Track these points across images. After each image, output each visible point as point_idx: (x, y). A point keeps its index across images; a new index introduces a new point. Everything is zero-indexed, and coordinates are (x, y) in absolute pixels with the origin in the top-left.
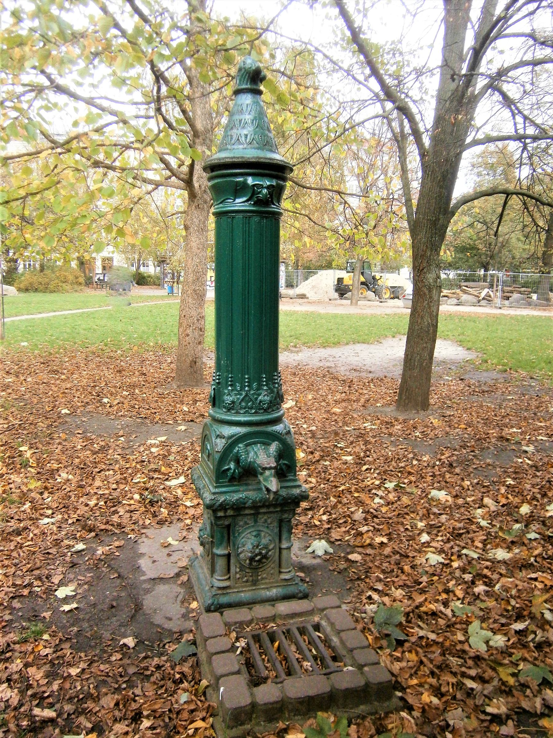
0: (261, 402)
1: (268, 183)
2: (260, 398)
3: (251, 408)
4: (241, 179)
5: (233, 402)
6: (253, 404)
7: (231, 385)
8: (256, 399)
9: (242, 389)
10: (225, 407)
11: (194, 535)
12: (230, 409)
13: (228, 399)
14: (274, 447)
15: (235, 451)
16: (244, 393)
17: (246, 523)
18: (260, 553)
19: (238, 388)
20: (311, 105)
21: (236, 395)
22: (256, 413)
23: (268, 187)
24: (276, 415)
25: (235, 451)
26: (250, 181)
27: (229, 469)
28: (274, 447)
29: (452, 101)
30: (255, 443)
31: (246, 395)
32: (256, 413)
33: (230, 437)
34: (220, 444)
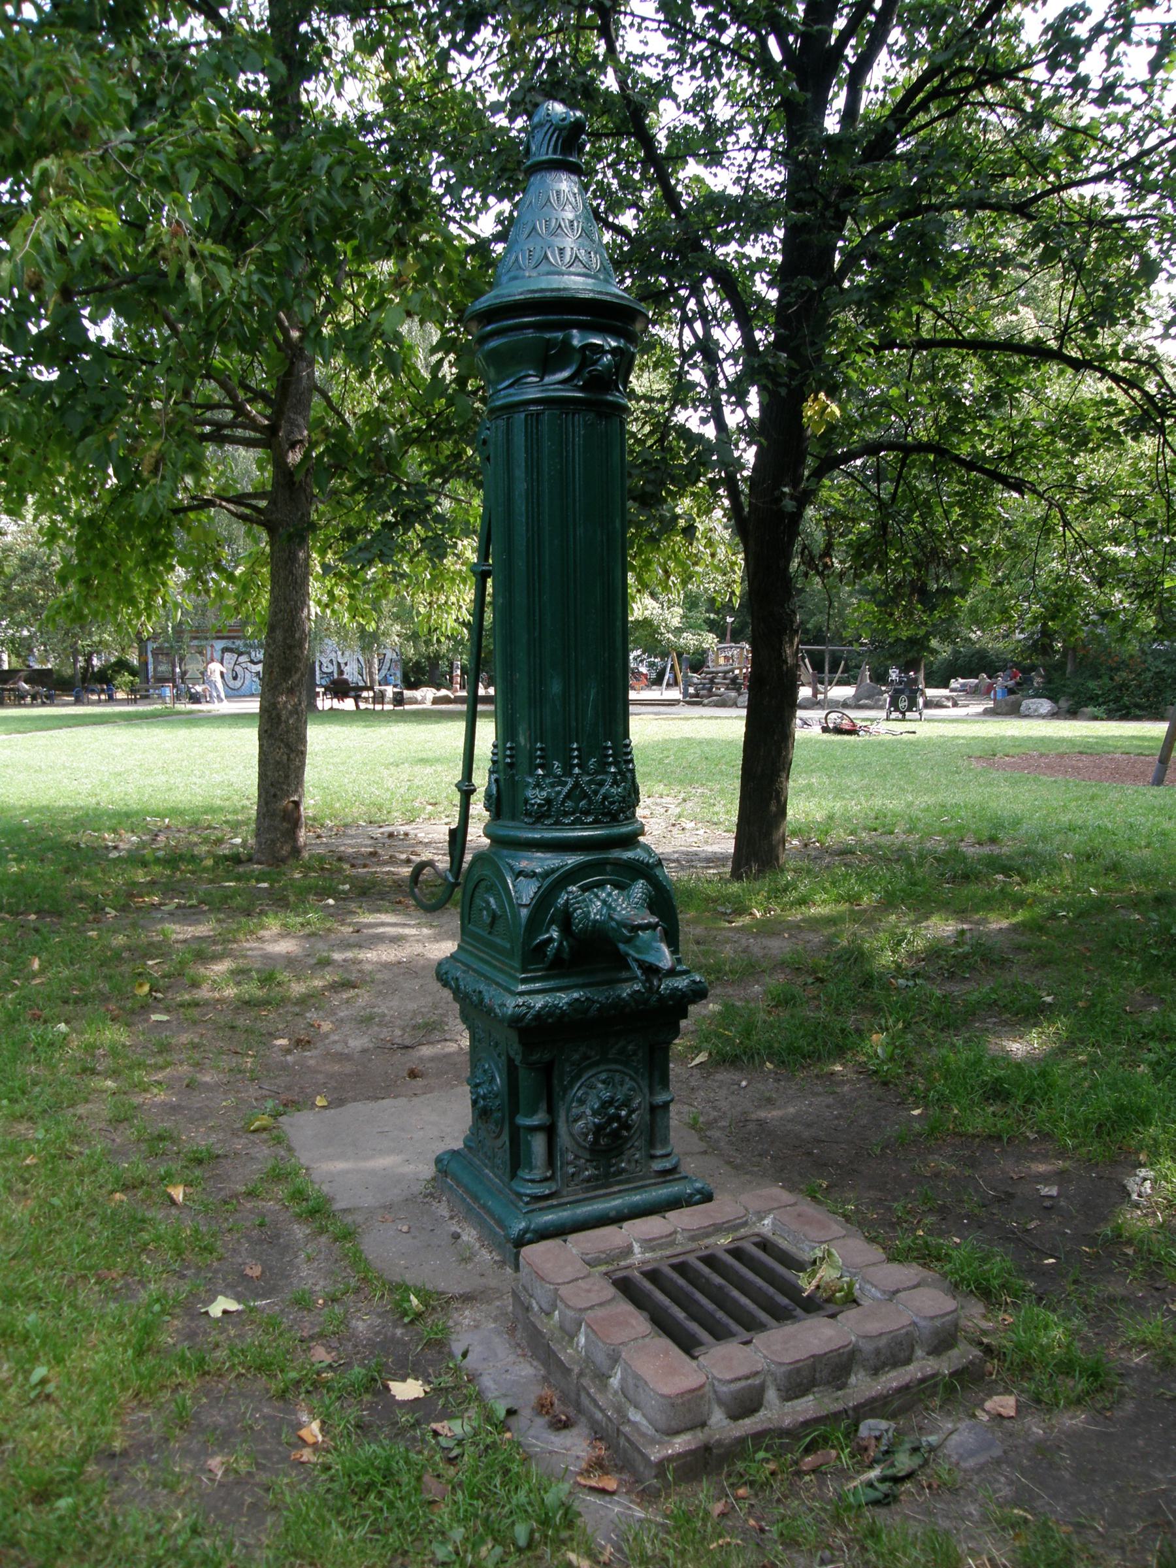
0: (605, 798)
1: (614, 344)
2: (603, 791)
3: (587, 813)
4: (560, 335)
5: (548, 801)
6: (590, 802)
7: (542, 766)
8: (596, 793)
9: (568, 772)
10: (528, 814)
11: (929, 923)
12: (540, 816)
13: (536, 796)
14: (639, 888)
15: (561, 901)
16: (570, 782)
17: (586, 1057)
18: (617, 1117)
19: (559, 772)
20: (424, 554)
21: (552, 785)
22: (595, 822)
23: (613, 351)
24: (624, 830)
25: (561, 901)
26: (577, 339)
27: (551, 940)
28: (639, 888)
29: (774, 366)
30: (600, 885)
31: (576, 785)
32: (595, 822)
33: (546, 874)
34: (527, 891)
